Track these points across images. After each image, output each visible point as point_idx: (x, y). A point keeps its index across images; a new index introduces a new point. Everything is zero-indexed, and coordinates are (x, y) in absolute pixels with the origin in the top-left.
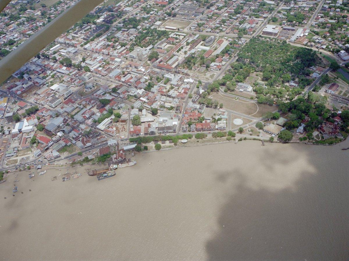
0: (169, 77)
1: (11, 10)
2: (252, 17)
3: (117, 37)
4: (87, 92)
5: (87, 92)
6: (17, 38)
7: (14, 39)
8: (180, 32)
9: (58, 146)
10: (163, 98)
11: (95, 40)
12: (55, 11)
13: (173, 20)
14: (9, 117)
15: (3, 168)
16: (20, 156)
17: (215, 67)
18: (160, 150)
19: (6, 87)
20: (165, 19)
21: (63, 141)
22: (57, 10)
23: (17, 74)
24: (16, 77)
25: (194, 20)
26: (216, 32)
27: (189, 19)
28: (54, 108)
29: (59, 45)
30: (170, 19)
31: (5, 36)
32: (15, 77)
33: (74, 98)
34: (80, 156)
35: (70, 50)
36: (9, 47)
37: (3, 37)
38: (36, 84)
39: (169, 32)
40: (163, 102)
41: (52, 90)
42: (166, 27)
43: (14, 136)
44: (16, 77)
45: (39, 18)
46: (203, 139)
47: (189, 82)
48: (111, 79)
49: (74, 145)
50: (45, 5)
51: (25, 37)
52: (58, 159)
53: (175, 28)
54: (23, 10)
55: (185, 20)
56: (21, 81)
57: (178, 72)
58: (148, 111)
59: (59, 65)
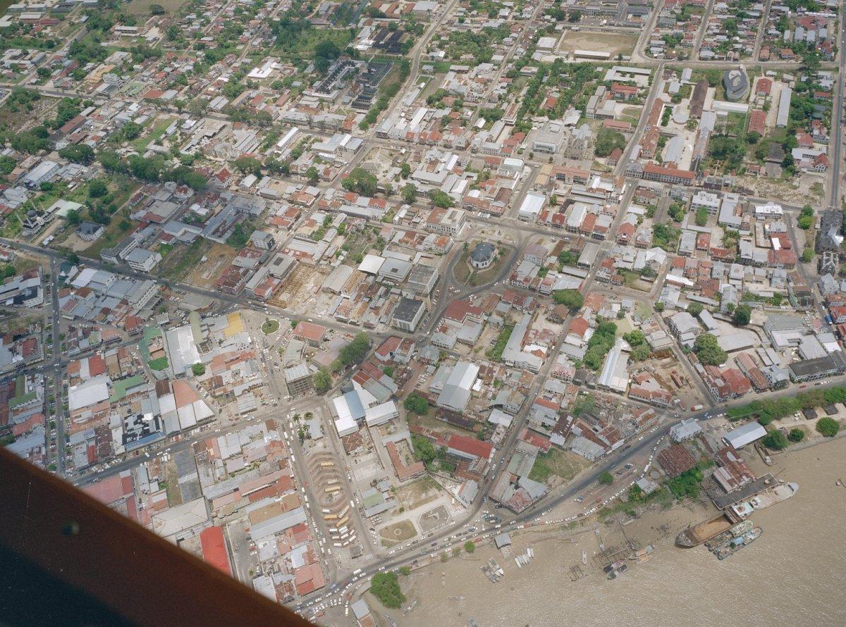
0: (704, 202)
1: (60, 28)
2: (798, 9)
3: (451, 92)
4: (480, 269)
5: (480, 269)
6: (139, 115)
7: (133, 118)
8: (627, 65)
9: (520, 462)
10: (737, 271)
11: (391, 103)
12: (204, 26)
13: (579, 30)
14: (295, 382)
15: (378, 556)
16: (411, 508)
17: (807, 160)
18: (836, 436)
19: (204, 276)
20: (557, 28)
21: (530, 441)
22: (208, 22)
23: (219, 232)
24: (221, 241)
25: (639, 27)
26: (728, 59)
27: (625, 26)
28: (412, 333)
29: (295, 129)
30: (570, 28)
31: (93, 111)
32: (214, 242)
33: (455, 294)
34: (605, 486)
35: (343, 144)
36: (129, 144)
37: (88, 115)
38: (303, 260)
39: (598, 65)
40: (740, 283)
41: (369, 274)
42: (577, 52)
43: (351, 441)
44: (221, 241)
45: (167, 47)
46: (251, 22)
47: (772, 213)
48: (526, 223)
49: (560, 451)
50: (160, 7)
51: (163, 110)
52: (425, 506)
53: (607, 55)
54: (99, 25)
55: (613, 28)
56: (249, 255)
57: (716, 185)
58: (715, 315)
59: (342, 194)
